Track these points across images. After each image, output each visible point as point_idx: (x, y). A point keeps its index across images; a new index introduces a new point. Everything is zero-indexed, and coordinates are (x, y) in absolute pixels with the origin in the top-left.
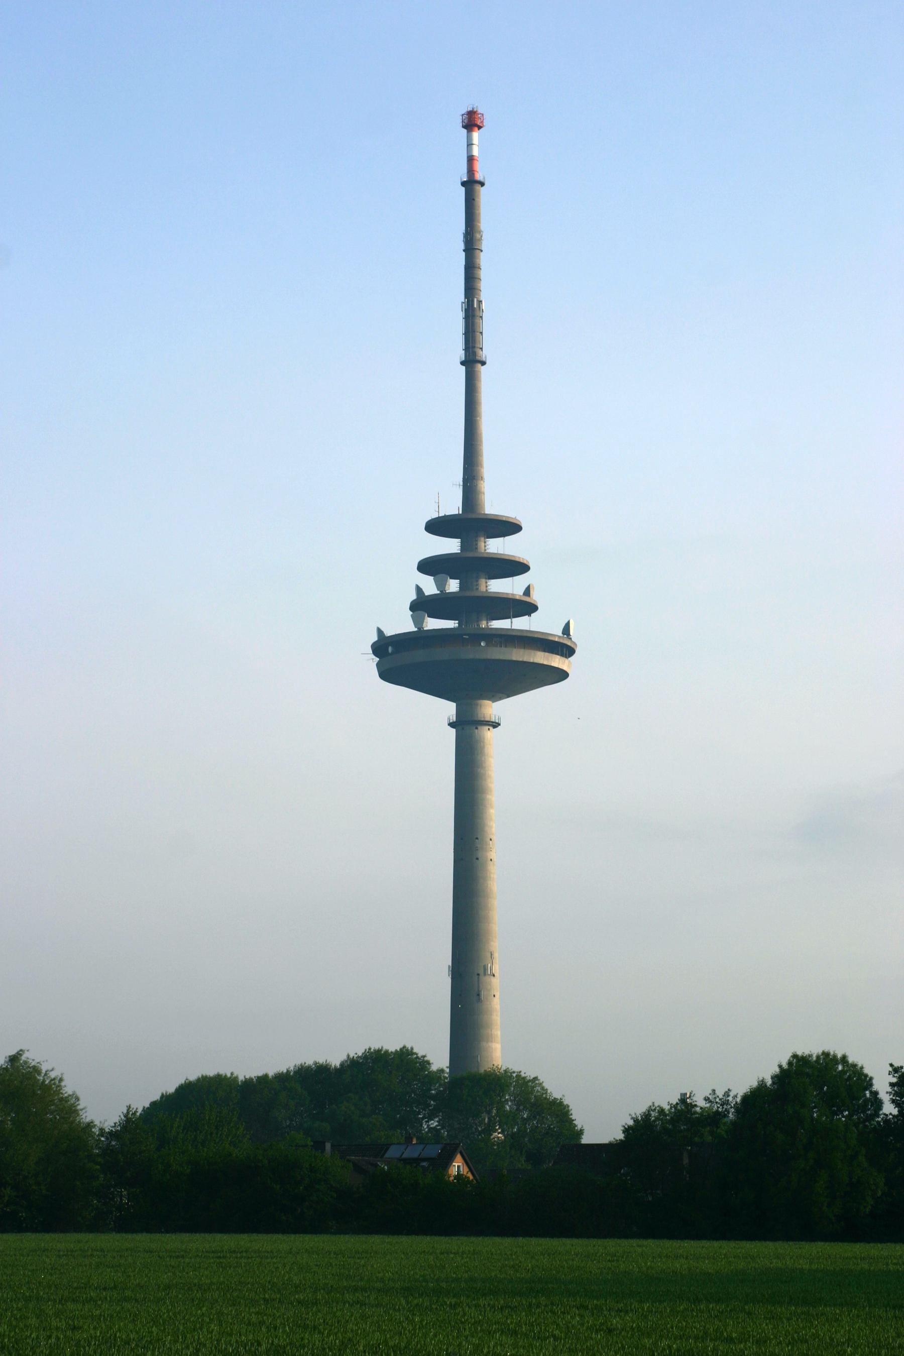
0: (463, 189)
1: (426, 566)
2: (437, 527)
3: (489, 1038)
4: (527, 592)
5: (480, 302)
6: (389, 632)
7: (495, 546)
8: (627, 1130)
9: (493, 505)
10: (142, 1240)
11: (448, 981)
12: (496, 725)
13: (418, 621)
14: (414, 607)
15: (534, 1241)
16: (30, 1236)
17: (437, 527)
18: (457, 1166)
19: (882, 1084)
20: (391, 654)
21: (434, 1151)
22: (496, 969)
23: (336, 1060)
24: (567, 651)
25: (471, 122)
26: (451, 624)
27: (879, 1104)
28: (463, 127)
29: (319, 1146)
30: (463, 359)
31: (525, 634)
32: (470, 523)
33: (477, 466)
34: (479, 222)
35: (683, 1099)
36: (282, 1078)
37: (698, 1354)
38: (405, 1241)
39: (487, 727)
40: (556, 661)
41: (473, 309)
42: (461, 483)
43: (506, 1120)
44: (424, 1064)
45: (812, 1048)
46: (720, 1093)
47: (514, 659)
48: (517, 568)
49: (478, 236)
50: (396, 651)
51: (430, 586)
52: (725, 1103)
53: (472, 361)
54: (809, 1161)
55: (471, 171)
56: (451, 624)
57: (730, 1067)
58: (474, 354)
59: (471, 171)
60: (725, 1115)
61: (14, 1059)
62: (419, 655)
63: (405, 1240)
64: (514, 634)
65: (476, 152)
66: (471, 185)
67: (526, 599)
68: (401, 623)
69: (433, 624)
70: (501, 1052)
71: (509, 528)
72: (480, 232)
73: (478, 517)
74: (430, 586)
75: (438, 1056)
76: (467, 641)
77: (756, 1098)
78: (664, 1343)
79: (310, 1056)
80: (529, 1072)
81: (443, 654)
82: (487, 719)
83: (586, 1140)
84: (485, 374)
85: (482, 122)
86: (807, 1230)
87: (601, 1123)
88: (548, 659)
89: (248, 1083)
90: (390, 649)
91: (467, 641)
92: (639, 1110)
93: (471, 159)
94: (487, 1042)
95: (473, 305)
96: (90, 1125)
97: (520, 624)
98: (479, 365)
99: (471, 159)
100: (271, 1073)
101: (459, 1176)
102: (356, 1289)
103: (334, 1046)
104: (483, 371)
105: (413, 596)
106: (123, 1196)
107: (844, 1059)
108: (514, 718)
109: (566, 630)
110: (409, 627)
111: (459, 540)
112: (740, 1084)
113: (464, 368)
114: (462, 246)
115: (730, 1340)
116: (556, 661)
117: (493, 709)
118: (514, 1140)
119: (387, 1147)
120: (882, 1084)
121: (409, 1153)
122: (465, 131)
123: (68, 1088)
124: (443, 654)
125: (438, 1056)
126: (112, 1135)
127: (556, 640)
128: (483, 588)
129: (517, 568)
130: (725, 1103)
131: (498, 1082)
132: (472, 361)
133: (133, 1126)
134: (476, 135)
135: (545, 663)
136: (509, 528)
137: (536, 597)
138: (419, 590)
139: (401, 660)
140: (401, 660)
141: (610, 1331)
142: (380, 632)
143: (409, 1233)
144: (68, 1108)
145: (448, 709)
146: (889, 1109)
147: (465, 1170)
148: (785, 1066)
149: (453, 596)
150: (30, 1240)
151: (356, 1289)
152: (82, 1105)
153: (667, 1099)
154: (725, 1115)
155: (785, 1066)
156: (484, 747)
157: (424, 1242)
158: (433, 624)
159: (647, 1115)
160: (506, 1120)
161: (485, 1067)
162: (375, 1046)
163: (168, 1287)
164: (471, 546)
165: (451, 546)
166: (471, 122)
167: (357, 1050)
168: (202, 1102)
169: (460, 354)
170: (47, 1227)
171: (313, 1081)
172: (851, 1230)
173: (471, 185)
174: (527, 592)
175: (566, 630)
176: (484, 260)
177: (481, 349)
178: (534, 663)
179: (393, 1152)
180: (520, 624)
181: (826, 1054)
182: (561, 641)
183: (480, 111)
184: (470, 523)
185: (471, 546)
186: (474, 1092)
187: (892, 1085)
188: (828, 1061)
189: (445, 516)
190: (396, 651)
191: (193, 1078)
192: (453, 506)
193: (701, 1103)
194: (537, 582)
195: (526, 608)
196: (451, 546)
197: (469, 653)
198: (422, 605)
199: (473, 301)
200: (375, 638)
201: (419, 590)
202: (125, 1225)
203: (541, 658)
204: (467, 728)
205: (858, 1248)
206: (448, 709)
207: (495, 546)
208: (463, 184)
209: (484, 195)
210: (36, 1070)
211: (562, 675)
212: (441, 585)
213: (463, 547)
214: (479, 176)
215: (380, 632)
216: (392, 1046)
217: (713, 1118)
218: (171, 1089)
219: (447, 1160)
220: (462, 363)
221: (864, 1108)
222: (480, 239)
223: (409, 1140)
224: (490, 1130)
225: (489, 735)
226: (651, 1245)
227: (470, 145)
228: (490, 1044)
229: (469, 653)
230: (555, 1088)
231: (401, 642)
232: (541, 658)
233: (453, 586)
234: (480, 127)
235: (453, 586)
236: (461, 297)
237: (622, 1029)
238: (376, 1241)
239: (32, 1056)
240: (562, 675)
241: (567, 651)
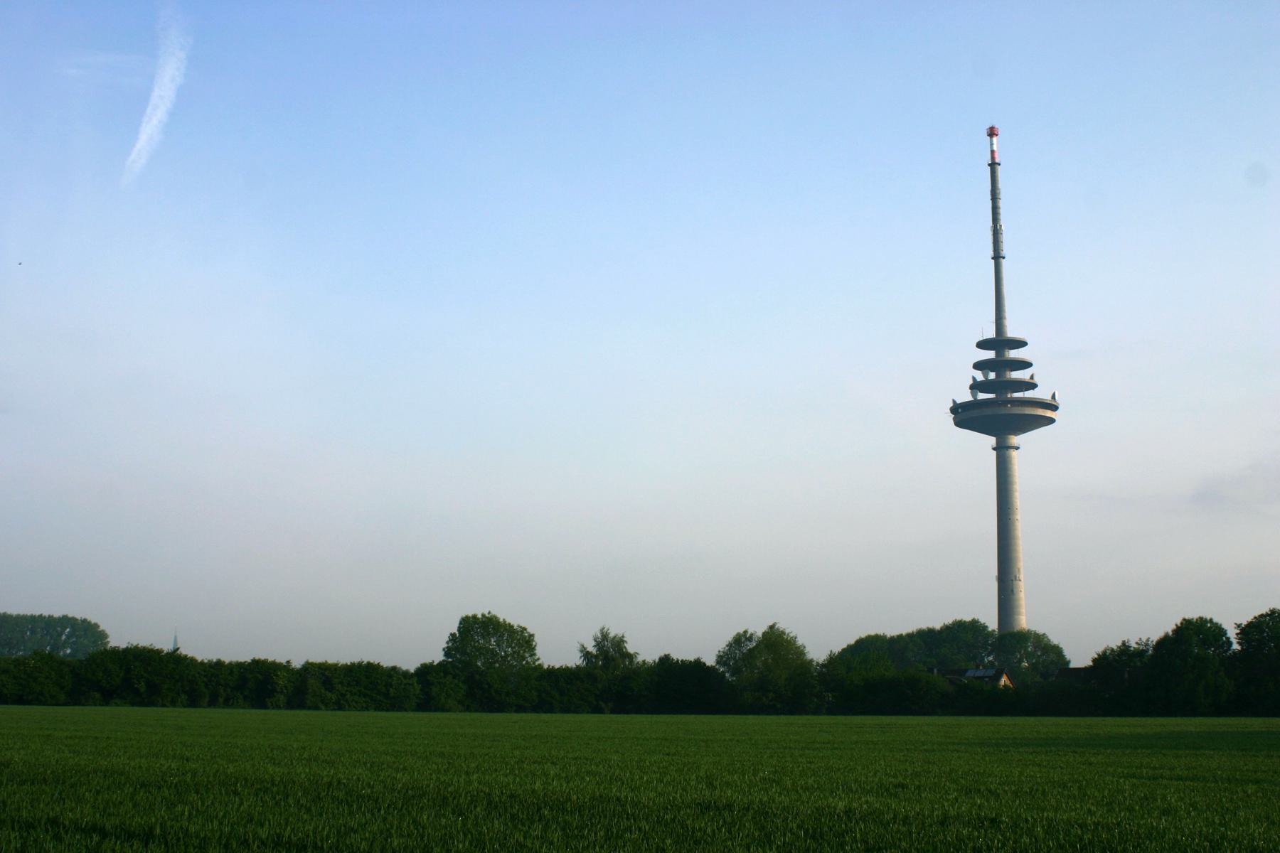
1: (978, 366)
2: (982, 345)
3: (1019, 614)
4: (1032, 377)
7: (1014, 354)
8: (1094, 661)
9: (1012, 332)
10: (840, 719)
12: (1017, 448)
13: (974, 395)
14: (972, 387)
15: (1047, 718)
16: (783, 717)
17: (982, 345)
18: (1004, 680)
19: (1232, 633)
21: (991, 672)
22: (1022, 577)
23: (938, 626)
24: (1054, 408)
25: (992, 133)
26: (991, 396)
27: (1230, 644)
29: (931, 670)
32: (1000, 343)
35: (1124, 643)
36: (910, 636)
38: (978, 719)
40: (1049, 414)
43: (1029, 656)
44: (985, 627)
45: (1193, 614)
46: (1144, 640)
48: (1025, 365)
51: (980, 376)
52: (1147, 645)
53: (997, 257)
54: (1189, 674)
55: (993, 158)
56: (991, 396)
57: (1148, 625)
59: (993, 158)
60: (1146, 651)
61: (772, 627)
62: (975, 413)
63: (978, 718)
65: (995, 148)
66: (993, 165)
68: (965, 396)
69: (982, 396)
70: (1025, 620)
71: (1021, 344)
74: (980, 376)
75: (992, 623)
76: (1000, 405)
77: (1164, 642)
78: (1120, 770)
79: (925, 624)
80: (1040, 631)
81: (989, 411)
83: (1072, 665)
84: (1005, 263)
86: (1194, 713)
87: (1080, 656)
89: (892, 639)
91: (1000, 405)
92: (1100, 650)
93: (993, 152)
96: (812, 661)
97: (1029, 394)
99: (993, 152)
100: (904, 633)
101: (1005, 686)
102: (954, 744)
103: (937, 620)
104: (1003, 261)
106: (830, 697)
107: (1211, 620)
108: (1026, 444)
109: (1053, 397)
110: (970, 398)
112: (1155, 636)
115: (1155, 768)
116: (1049, 414)
117: (1015, 440)
118: (1034, 667)
119: (966, 671)
120: (1232, 633)
121: (979, 673)
123: (800, 642)
124: (989, 411)
125: (992, 623)
126: (823, 666)
129: (1025, 365)
130: (1147, 645)
131: (1024, 636)
132: (997, 257)
133: (834, 661)
134: (995, 139)
136: (1021, 344)
137: (1036, 380)
138: (974, 379)
139: (965, 416)
140: (965, 416)
141: (1090, 764)
143: (980, 715)
144: (800, 652)
146: (1236, 647)
147: (1008, 683)
148: (591, 648)
150: (783, 719)
151: (954, 744)
152: (807, 650)
153: (1115, 644)
154: (1146, 651)
155: (591, 648)
157: (988, 720)
158: (982, 396)
159: (1104, 652)
160: (1029, 656)
161: (1017, 629)
162: (959, 618)
163: (856, 742)
164: (1001, 353)
165: (990, 355)
166: (992, 133)
167: (949, 620)
168: (868, 648)
169: (991, 253)
170: (791, 713)
171: (927, 638)
172: (1217, 711)
173: (993, 165)
174: (1032, 377)
175: (1053, 397)
178: (1035, 415)
179: (970, 674)
180: (1029, 394)
181: (1201, 618)
184: (1000, 343)
185: (1001, 353)
186: (1010, 641)
188: (1202, 622)
191: (863, 636)
192: (990, 333)
193: (1134, 645)
194: (1036, 372)
195: (1031, 386)
196: (990, 355)
198: (976, 387)
201: (974, 379)
202: (831, 711)
203: (1041, 412)
204: (1002, 450)
205: (1221, 720)
206: (992, 440)
207: (1014, 354)
209: (1000, 169)
210: (783, 633)
211: (1052, 421)
212: (985, 375)
216: (968, 618)
217: (1140, 653)
218: (852, 642)
219: (998, 678)
221: (1222, 646)
223: (977, 667)
224: (1020, 661)
225: (1014, 454)
226: (1109, 720)
227: (992, 144)
229: (1003, 411)
230: (1055, 640)
231: (965, 406)
232: (1041, 412)
233: (992, 375)
235: (992, 375)
237: (1088, 608)
238: (963, 719)
239: (781, 626)
240: (1052, 421)
241: (1054, 408)
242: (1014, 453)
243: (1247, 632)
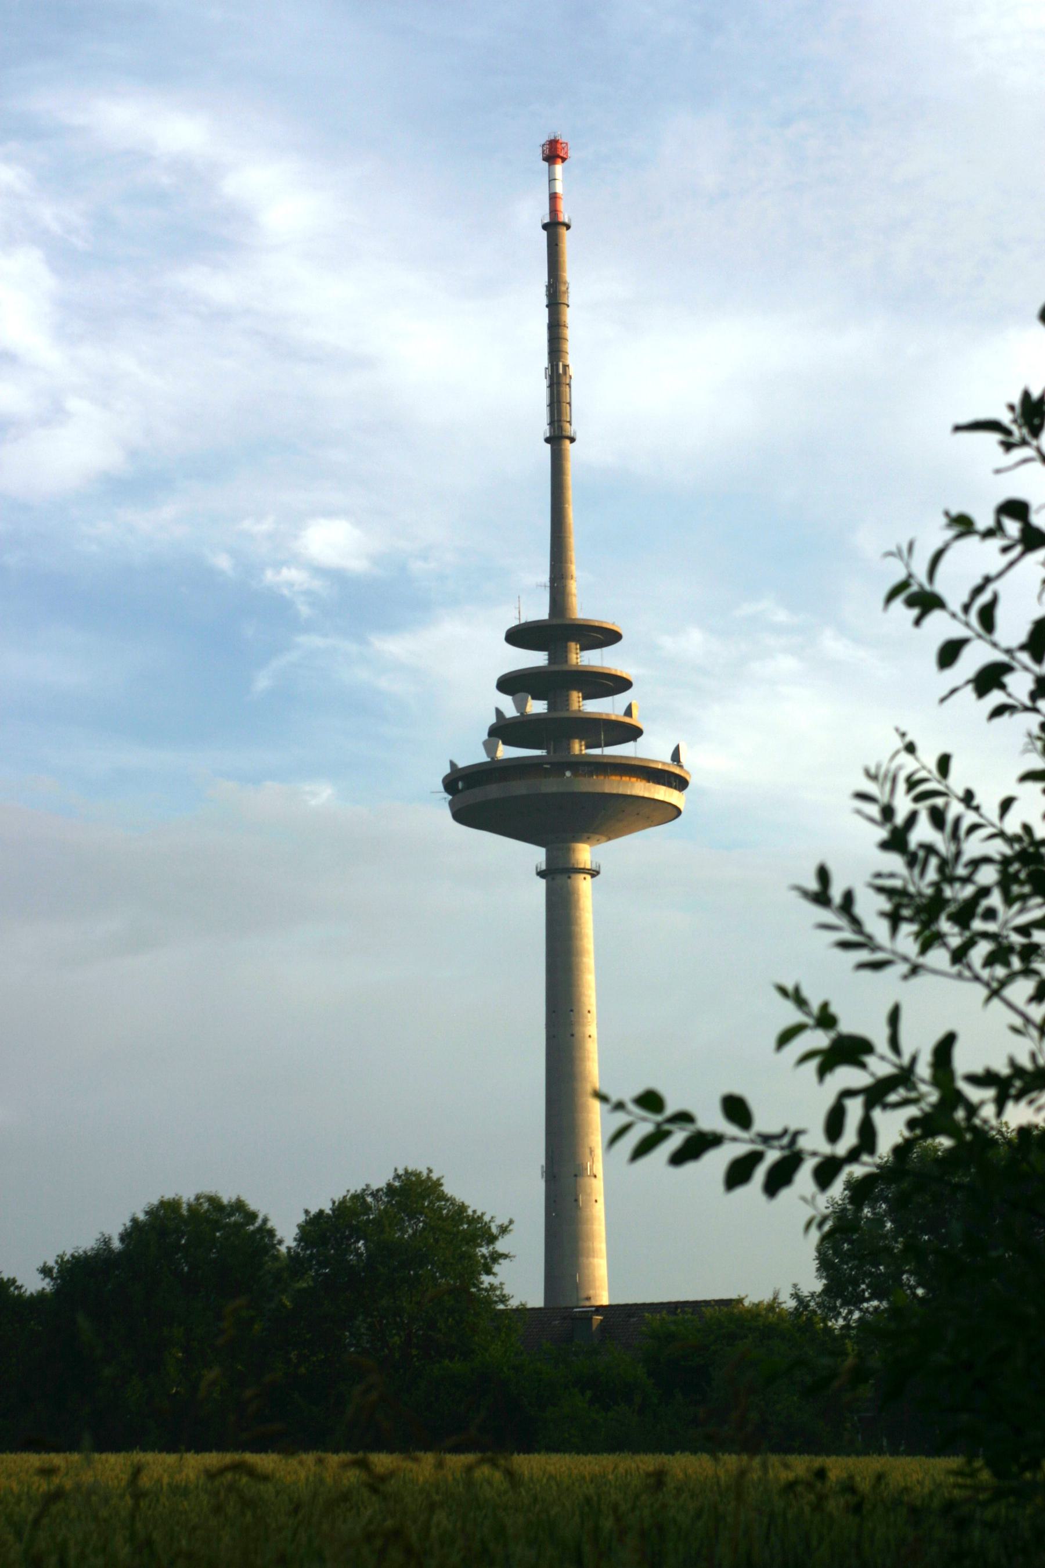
0: (545, 233)
2: (520, 636)
3: (590, 1253)
4: (629, 712)
5: (566, 366)
6: (461, 764)
9: (584, 607)
11: (541, 1185)
13: (490, 747)
17: (520, 636)
20: (462, 791)
25: (553, 153)
28: (545, 159)
30: (548, 435)
31: (619, 761)
32: (556, 632)
33: (566, 562)
34: (564, 271)
37: (63, 1564)
39: (582, 876)
41: (559, 375)
42: (548, 584)
45: (186, 1190)
47: (607, 791)
49: (563, 288)
50: (468, 786)
51: (508, 707)
55: (554, 210)
58: (561, 428)
59: (554, 210)
62: (494, 791)
64: (605, 761)
65: (559, 188)
67: (627, 720)
69: (505, 752)
71: (608, 637)
72: (565, 283)
73: (568, 622)
74: (508, 707)
81: (519, 788)
82: (582, 866)
85: (566, 153)
88: (649, 790)
90: (460, 785)
93: (553, 198)
94: (587, 1257)
95: (558, 369)
98: (567, 442)
99: (553, 198)
105: (492, 719)
109: (676, 756)
110: (482, 757)
111: (546, 653)
113: (549, 446)
114: (544, 301)
116: (662, 793)
117: (585, 854)
122: (546, 164)
124: (519, 788)
127: (660, 766)
128: (575, 706)
129: (620, 684)
134: (559, 168)
135: (647, 795)
136: (608, 637)
138: (499, 713)
139: (479, 797)
140: (479, 797)
142: (453, 765)
145: (537, 855)
149: (537, 718)
156: (578, 901)
158: (505, 752)
165: (538, 659)
166: (553, 153)
173: (554, 227)
174: (629, 712)
175: (676, 756)
176: (571, 316)
177: (570, 422)
182: (666, 768)
183: (563, 140)
187: (134, 1220)
189: (526, 623)
190: (468, 786)
192: (539, 611)
196: (538, 659)
197: (550, 786)
198: (503, 730)
199: (557, 366)
200: (447, 770)
201: (499, 713)
203: (641, 788)
204: (559, 875)
206: (537, 855)
208: (545, 227)
209: (569, 240)
212: (520, 706)
213: (551, 659)
214: (564, 217)
215: (453, 765)
220: (547, 440)
222: (566, 292)
227: (552, 180)
228: (591, 1260)
229: (550, 786)
232: (641, 788)
233: (537, 707)
234: (564, 160)
235: (537, 707)
236: (544, 361)
241: (680, 783)
242: (585, 886)
243: (316, 1229)
